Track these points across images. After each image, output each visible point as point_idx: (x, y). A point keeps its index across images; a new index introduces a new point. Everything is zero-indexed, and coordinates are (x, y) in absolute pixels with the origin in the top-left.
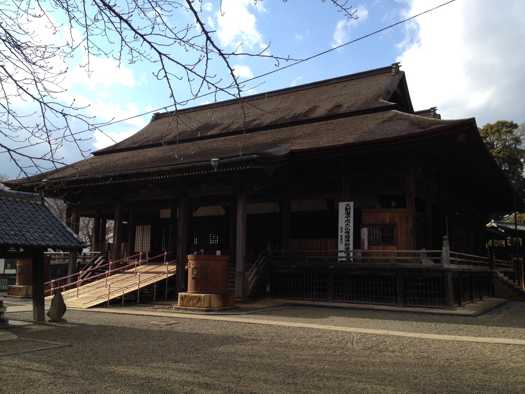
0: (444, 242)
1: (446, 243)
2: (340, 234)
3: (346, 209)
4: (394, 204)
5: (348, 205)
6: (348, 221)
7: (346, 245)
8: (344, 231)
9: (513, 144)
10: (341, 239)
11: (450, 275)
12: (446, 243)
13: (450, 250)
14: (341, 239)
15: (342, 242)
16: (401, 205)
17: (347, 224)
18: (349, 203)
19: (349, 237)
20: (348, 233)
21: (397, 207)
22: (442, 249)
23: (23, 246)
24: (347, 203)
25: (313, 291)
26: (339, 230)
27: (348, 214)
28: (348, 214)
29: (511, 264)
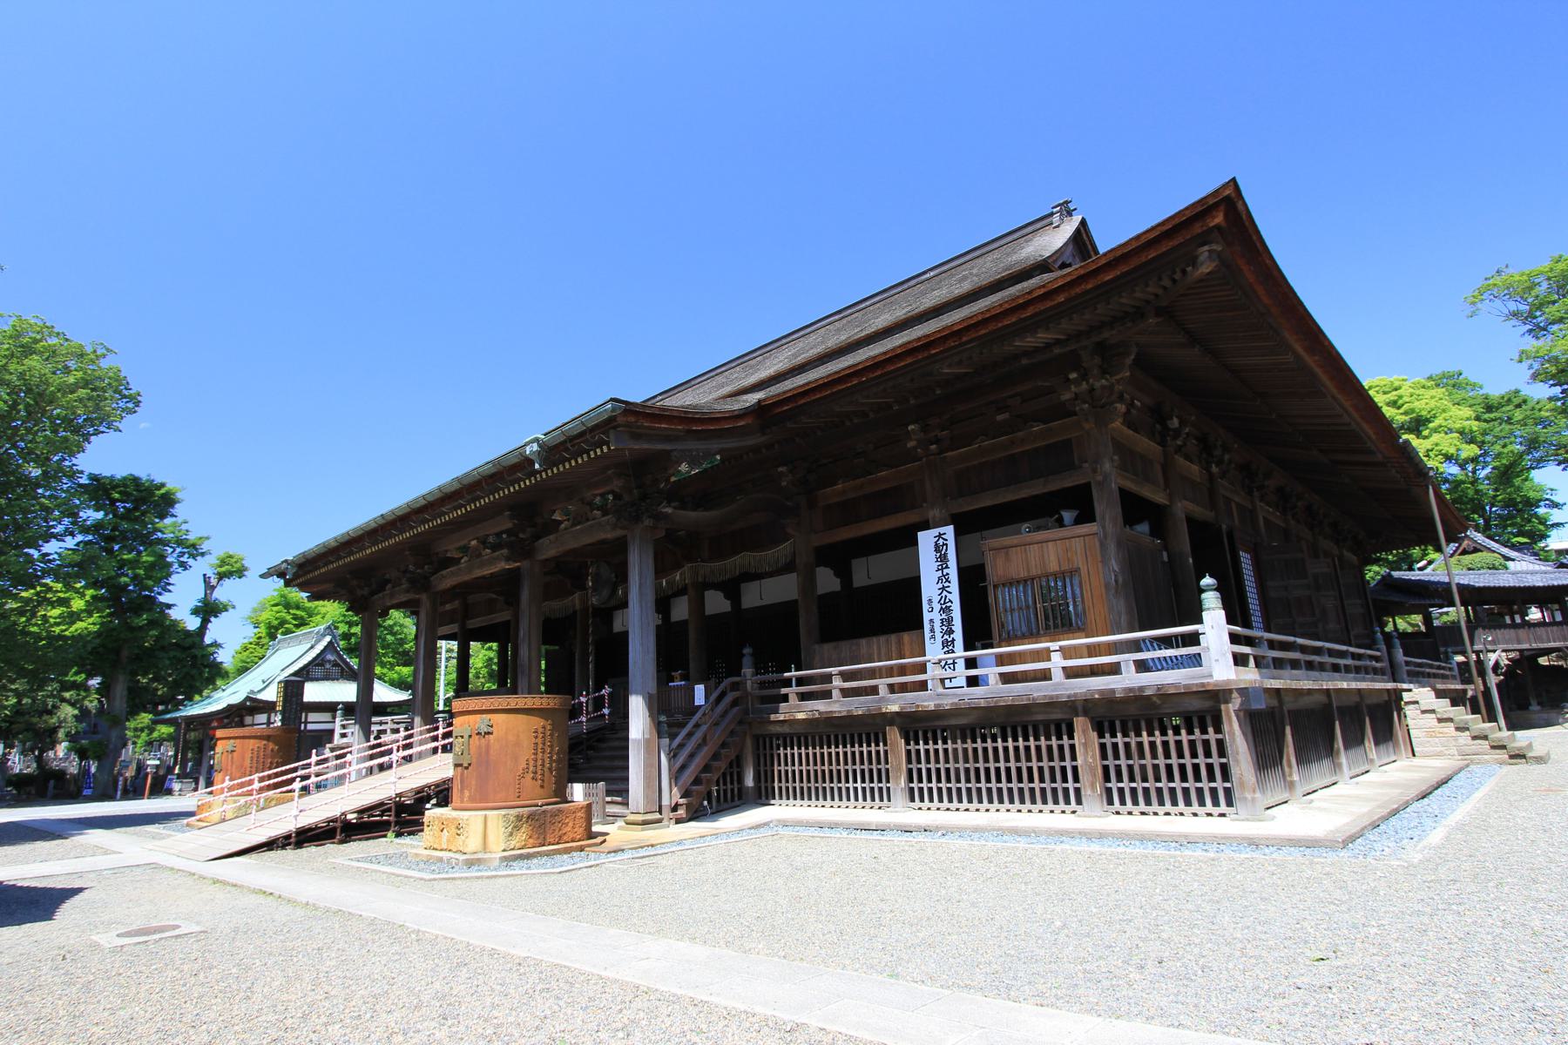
0: (1204, 596)
1: (1211, 600)
2: (927, 616)
3: (937, 548)
4: (1068, 516)
5: (940, 536)
6: (944, 578)
7: (945, 644)
8: (937, 607)
9: (1523, 618)
10: (932, 630)
11: (1236, 703)
12: (1211, 600)
13: (1230, 621)
14: (932, 630)
15: (933, 637)
16: (1086, 516)
17: (943, 588)
18: (942, 530)
19: (950, 621)
20: (946, 610)
21: (1078, 521)
22: (1200, 621)
23: (1506, 626)
24: (935, 532)
25: (855, 781)
26: (925, 607)
27: (943, 559)
28: (943, 559)
29: (1377, 659)
